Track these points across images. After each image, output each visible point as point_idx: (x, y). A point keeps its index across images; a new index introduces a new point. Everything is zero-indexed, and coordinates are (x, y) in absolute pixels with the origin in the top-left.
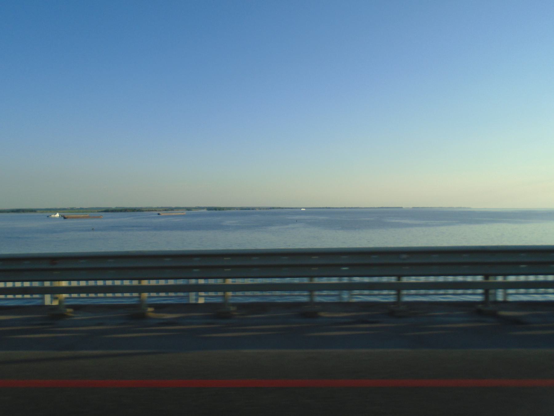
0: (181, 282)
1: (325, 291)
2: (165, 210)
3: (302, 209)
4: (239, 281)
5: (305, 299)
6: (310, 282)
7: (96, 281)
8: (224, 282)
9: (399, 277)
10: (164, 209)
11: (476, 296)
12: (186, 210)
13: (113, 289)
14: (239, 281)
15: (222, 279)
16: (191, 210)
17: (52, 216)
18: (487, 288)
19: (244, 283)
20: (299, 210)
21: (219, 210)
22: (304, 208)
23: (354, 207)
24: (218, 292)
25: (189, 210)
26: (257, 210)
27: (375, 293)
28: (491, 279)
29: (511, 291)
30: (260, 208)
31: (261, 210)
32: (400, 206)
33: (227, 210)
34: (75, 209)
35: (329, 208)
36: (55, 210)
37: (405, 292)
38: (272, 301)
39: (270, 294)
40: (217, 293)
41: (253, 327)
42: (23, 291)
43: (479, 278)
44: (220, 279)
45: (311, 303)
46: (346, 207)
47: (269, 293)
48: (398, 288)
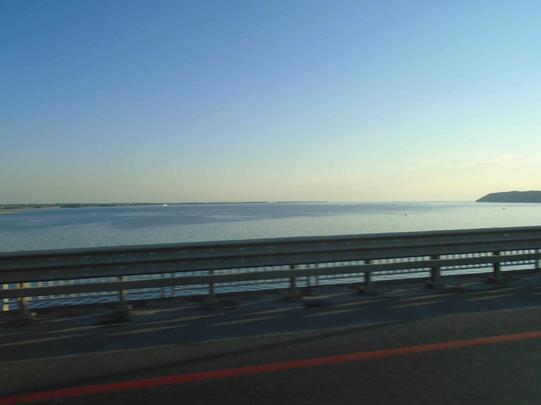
0: (157, 277)
2: (7, 208)
3: (164, 205)
4: (135, 278)
5: (205, 293)
6: (291, 270)
8: (121, 280)
9: (211, 270)
10: (3, 207)
12: (34, 208)
14: (135, 278)
18: (293, 276)
21: (86, 206)
22: (166, 204)
24: (101, 292)
25: (37, 208)
27: (329, 277)
29: (321, 277)
30: (122, 205)
31: (131, 206)
33: (84, 207)
35: (197, 203)
37: (216, 285)
40: (59, 296)
41: (264, 312)
43: (286, 268)
45: (212, 295)
46: (214, 202)
47: (127, 291)
48: (211, 281)
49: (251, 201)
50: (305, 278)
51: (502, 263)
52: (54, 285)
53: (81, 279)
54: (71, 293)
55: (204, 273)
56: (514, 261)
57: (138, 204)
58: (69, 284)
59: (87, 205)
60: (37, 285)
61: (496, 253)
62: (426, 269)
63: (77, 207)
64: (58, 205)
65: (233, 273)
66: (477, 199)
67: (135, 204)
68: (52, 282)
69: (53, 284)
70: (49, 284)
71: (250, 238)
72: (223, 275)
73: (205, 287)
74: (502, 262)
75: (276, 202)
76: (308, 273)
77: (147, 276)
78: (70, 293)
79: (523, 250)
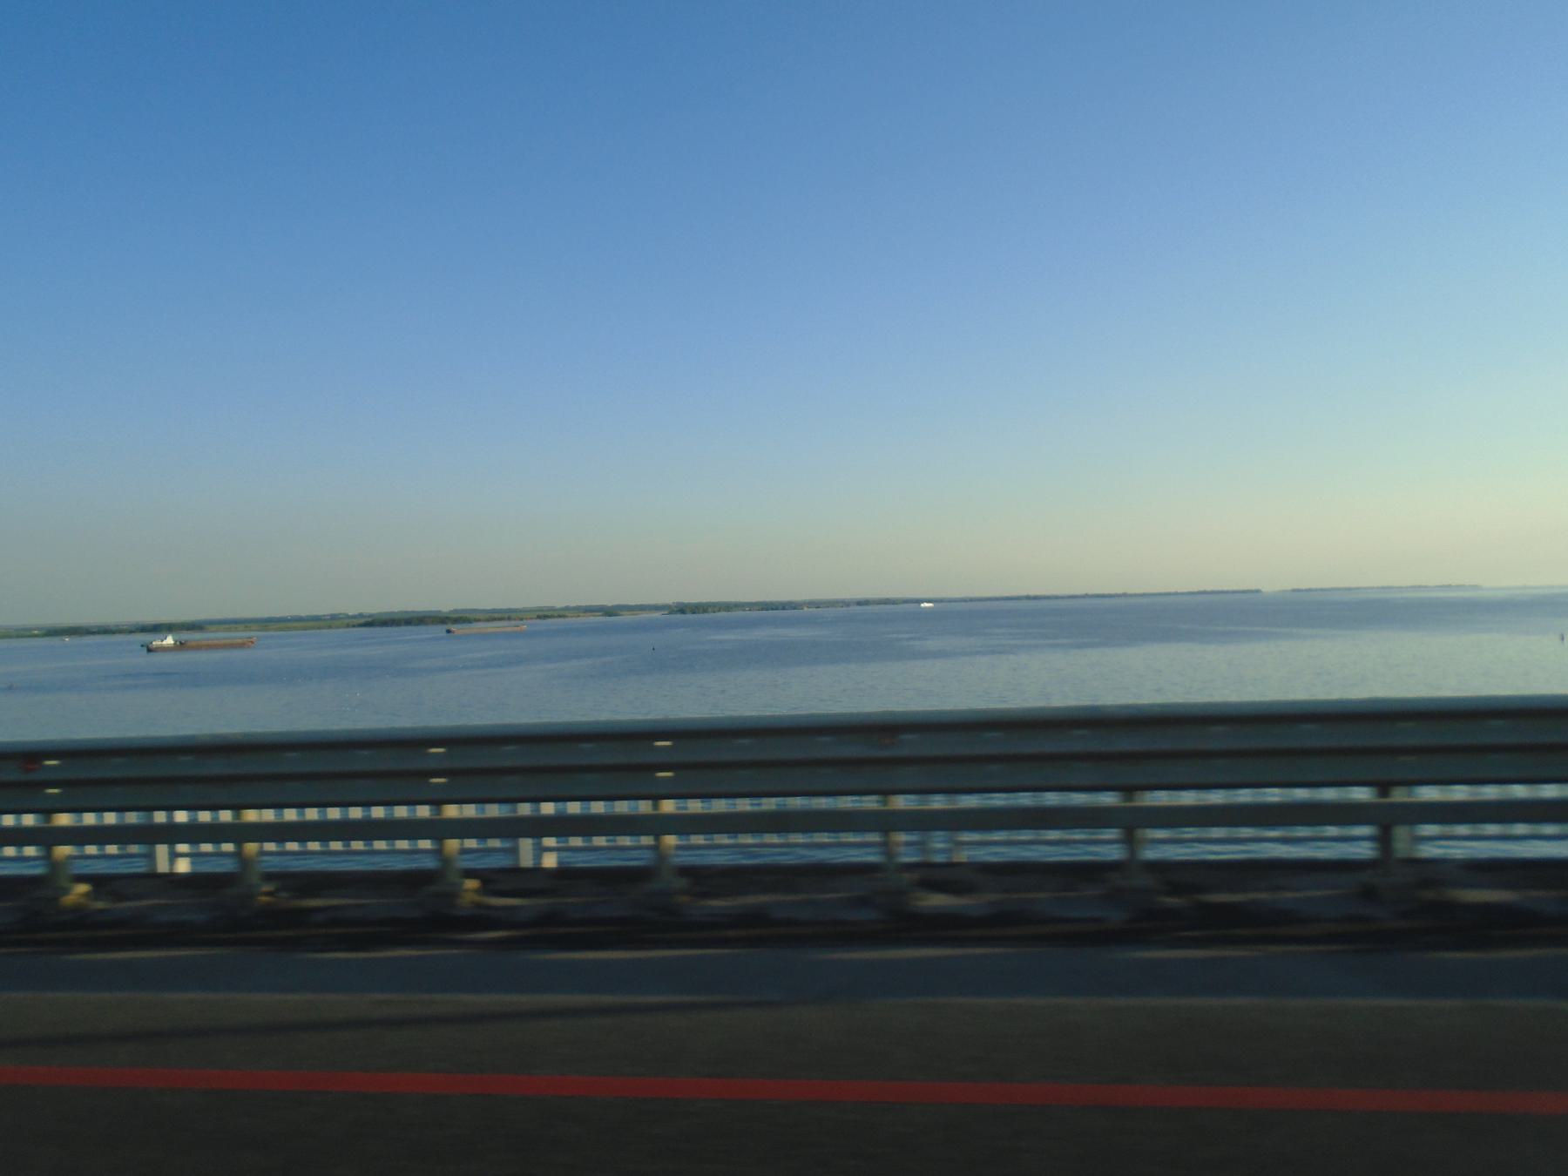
0: (494, 811)
3: (922, 605)
7: (412, 807)
11: (1358, 844)
12: (602, 615)
17: (154, 643)
18: (1386, 820)
20: (912, 605)
22: (928, 601)
23: (1209, 588)
24: (739, 835)
25: (610, 616)
26: (806, 609)
28: (1399, 796)
29: (967, 837)
30: (817, 604)
32: (1254, 588)
33: (719, 611)
34: (342, 618)
35: (1036, 598)
36: (169, 628)
38: (283, 870)
39: (731, 841)
47: (829, 838)
48: (1131, 823)
53: (716, 800)
55: (1265, 793)
57: (866, 603)
58: (370, 816)
59: (727, 607)
64: (656, 608)
67: (860, 603)
71: (42, 738)
77: (773, 800)
78: (892, 831)
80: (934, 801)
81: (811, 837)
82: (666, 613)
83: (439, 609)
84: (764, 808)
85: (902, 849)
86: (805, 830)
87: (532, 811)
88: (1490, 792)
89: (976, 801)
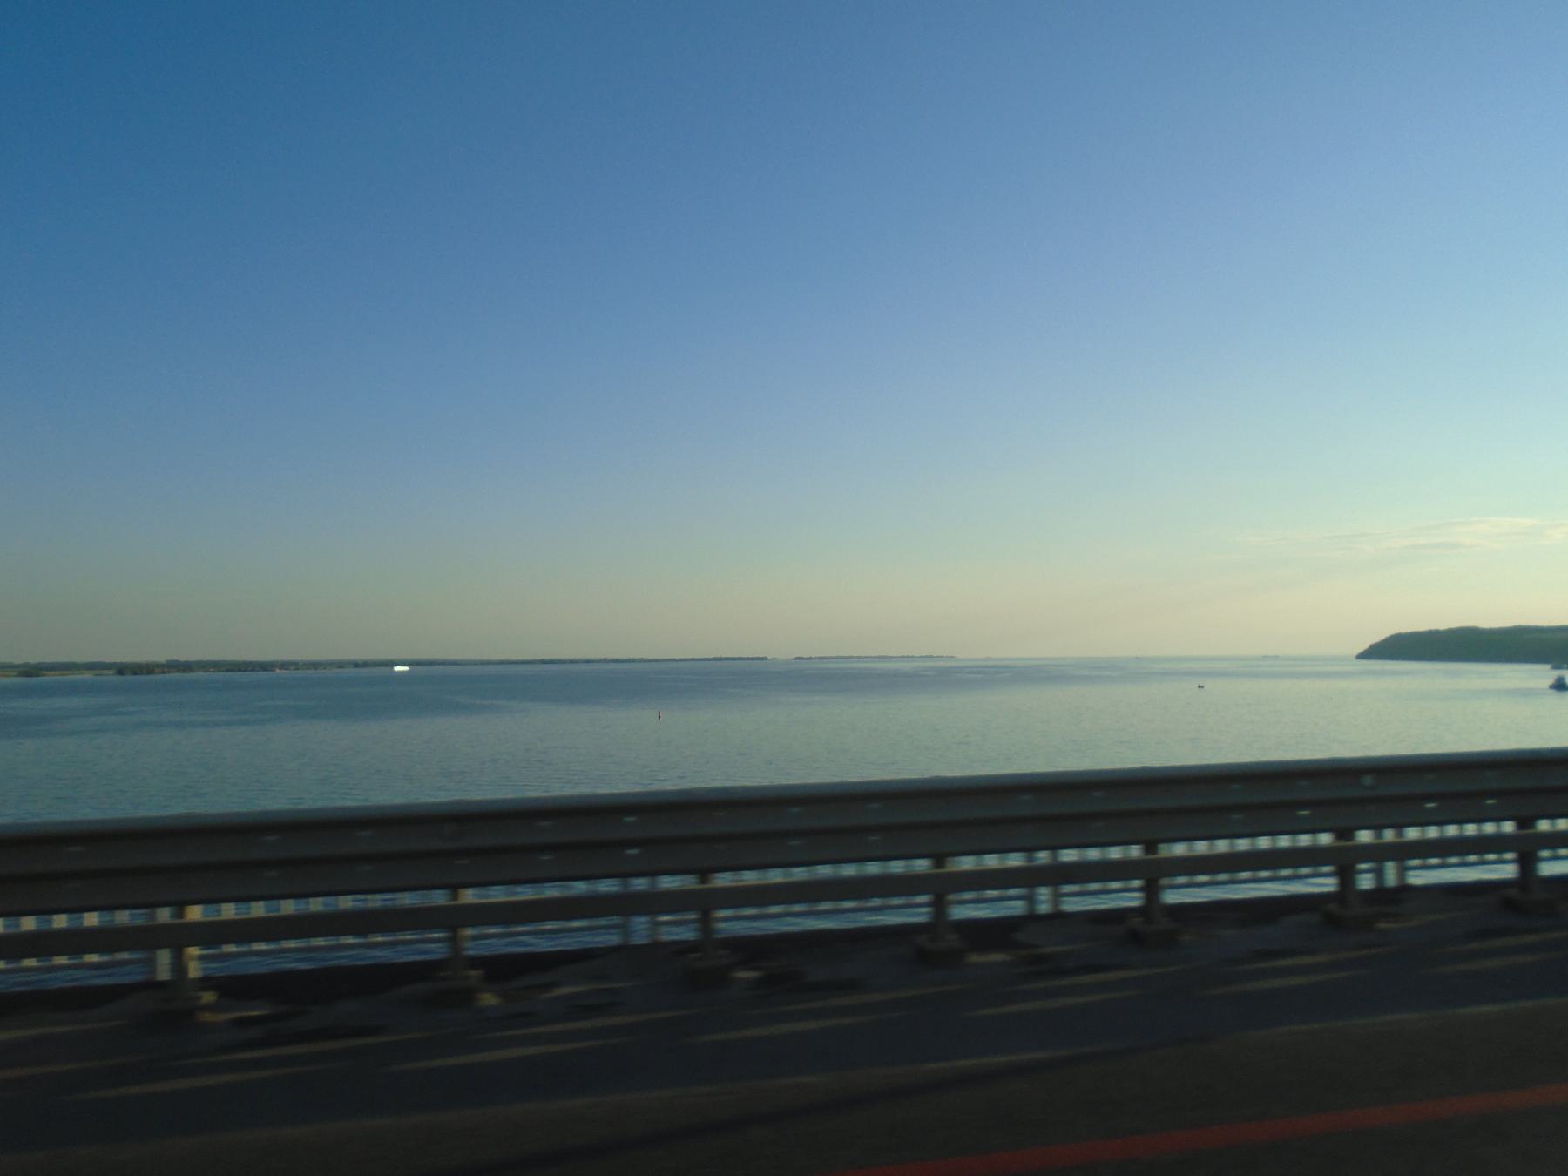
1: (550, 922)
4: (498, 895)
6: (700, 886)
9: (704, 874)
13: (1460, 847)
14: (498, 895)
15: (692, 876)
16: (38, 676)
18: (1344, 862)
19: (740, 884)
20: (384, 669)
21: (135, 673)
26: (278, 670)
27: (990, 896)
42: (77, 942)
43: (922, 865)
44: (828, 866)
45: (707, 941)
47: (325, 941)
48: (942, 888)
49: (610, 656)
50: (616, 920)
51: (1545, 853)
52: (236, 914)
54: (58, 955)
56: (1452, 855)
57: (365, 664)
58: (308, 909)
60: (18, 925)
61: (1344, 833)
62: (1013, 892)
63: (147, 674)
65: (747, 880)
66: (1364, 646)
67: (356, 665)
68: (232, 906)
69: (233, 912)
70: (223, 913)
72: (489, 903)
73: (431, 938)
74: (189, 946)
75: (793, 657)
76: (1378, 854)
79: (1273, 833)
80: (901, 868)
81: (395, 935)
82: (15, 674)
83: (1397, 632)
84: (371, 905)
85: (468, 944)
86: (414, 928)
87: (171, 916)
88: (317, 905)
89: (745, 878)
